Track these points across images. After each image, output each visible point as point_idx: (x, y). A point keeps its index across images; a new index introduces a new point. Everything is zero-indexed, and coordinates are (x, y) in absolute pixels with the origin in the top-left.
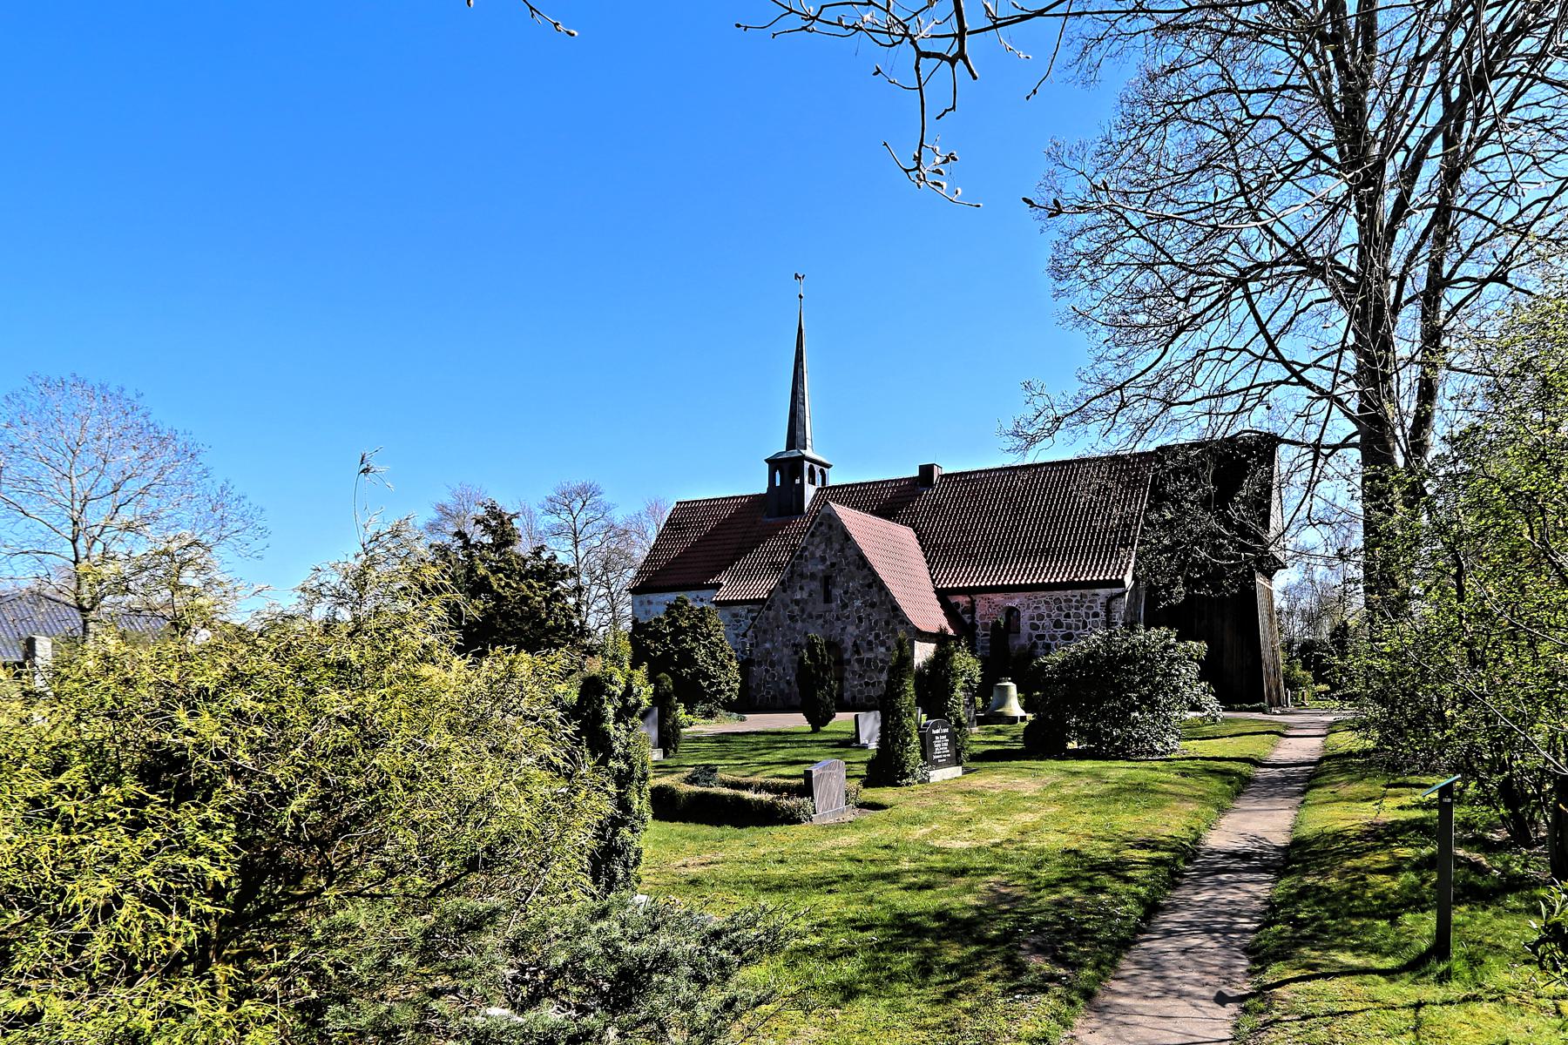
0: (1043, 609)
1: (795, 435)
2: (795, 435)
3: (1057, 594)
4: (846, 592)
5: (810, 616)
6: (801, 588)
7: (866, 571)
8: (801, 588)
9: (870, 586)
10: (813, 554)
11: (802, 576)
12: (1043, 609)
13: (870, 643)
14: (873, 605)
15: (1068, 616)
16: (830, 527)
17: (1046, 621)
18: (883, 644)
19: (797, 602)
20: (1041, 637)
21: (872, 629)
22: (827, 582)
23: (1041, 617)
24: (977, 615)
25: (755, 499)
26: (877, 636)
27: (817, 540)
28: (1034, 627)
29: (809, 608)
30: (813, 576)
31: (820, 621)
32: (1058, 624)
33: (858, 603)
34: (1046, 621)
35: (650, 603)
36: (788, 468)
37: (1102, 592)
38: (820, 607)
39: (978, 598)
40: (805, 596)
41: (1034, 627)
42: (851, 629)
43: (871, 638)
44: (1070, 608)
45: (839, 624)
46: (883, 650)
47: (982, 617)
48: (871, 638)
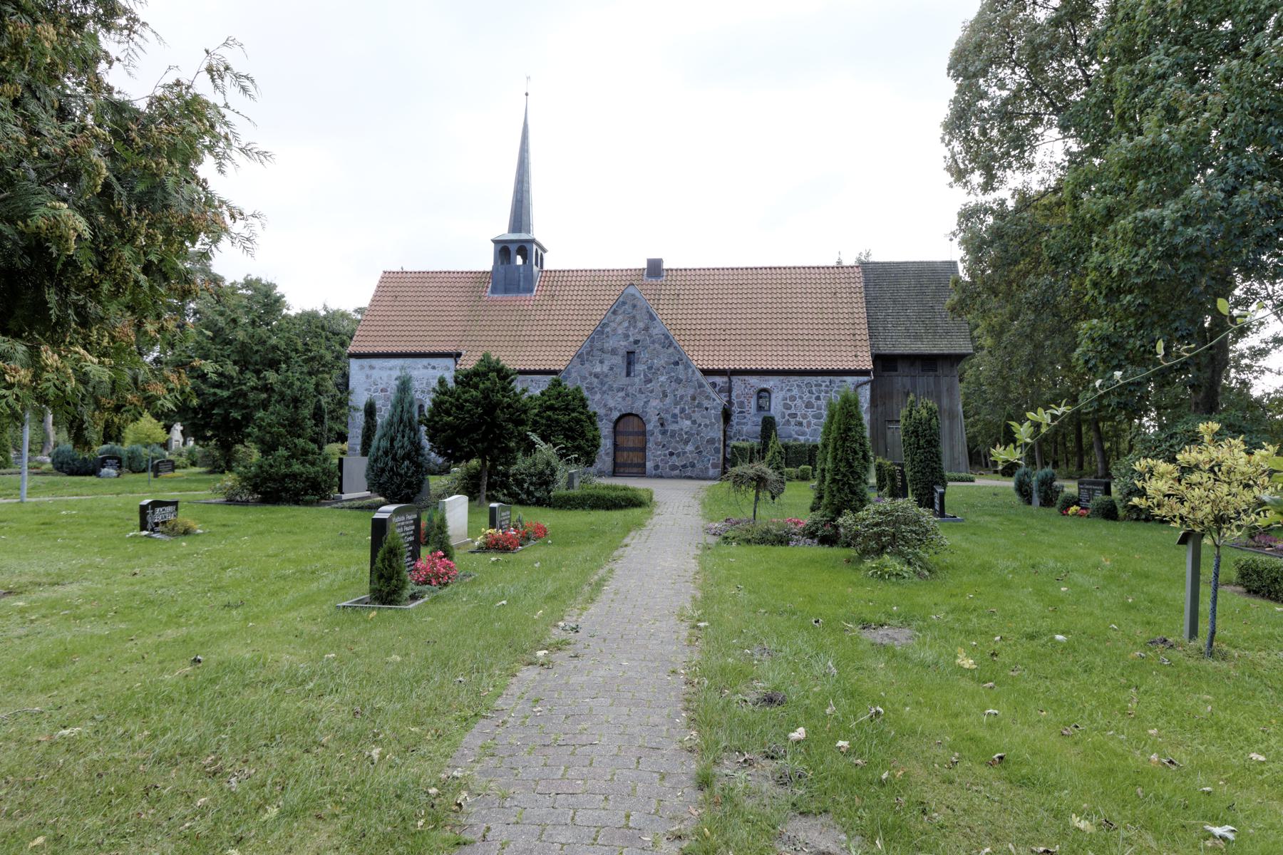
0: (795, 391)
1: (520, 216)
2: (520, 216)
3: (807, 379)
4: (650, 368)
5: (611, 388)
6: (601, 362)
7: (671, 350)
8: (601, 362)
9: (676, 363)
10: (615, 330)
11: (602, 350)
12: (795, 391)
13: (674, 416)
14: (679, 381)
15: (818, 398)
16: (634, 306)
17: (798, 402)
18: (689, 417)
19: (596, 376)
20: (794, 416)
21: (676, 404)
22: (630, 358)
23: (793, 398)
24: (734, 394)
25: (477, 277)
26: (683, 410)
27: (619, 318)
28: (787, 407)
29: (609, 380)
30: (614, 352)
31: (622, 394)
32: (809, 405)
33: (663, 379)
34: (798, 402)
35: (372, 367)
36: (516, 252)
37: (849, 379)
38: (624, 380)
39: (734, 379)
40: (606, 369)
41: (787, 407)
42: (655, 403)
43: (677, 411)
44: (820, 392)
45: (643, 398)
46: (688, 423)
47: (738, 396)
48: (677, 411)
